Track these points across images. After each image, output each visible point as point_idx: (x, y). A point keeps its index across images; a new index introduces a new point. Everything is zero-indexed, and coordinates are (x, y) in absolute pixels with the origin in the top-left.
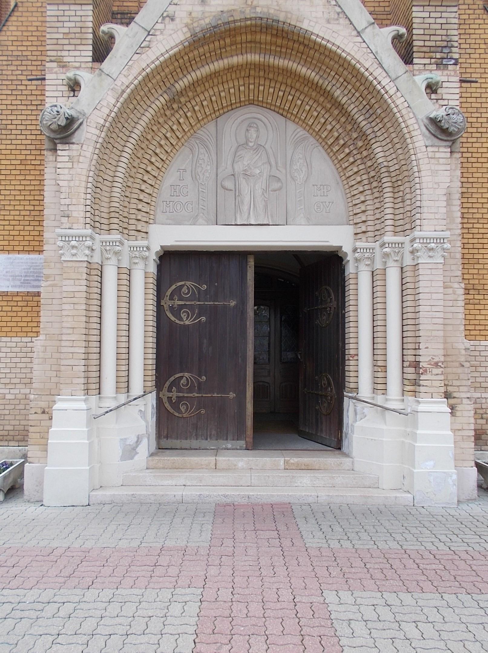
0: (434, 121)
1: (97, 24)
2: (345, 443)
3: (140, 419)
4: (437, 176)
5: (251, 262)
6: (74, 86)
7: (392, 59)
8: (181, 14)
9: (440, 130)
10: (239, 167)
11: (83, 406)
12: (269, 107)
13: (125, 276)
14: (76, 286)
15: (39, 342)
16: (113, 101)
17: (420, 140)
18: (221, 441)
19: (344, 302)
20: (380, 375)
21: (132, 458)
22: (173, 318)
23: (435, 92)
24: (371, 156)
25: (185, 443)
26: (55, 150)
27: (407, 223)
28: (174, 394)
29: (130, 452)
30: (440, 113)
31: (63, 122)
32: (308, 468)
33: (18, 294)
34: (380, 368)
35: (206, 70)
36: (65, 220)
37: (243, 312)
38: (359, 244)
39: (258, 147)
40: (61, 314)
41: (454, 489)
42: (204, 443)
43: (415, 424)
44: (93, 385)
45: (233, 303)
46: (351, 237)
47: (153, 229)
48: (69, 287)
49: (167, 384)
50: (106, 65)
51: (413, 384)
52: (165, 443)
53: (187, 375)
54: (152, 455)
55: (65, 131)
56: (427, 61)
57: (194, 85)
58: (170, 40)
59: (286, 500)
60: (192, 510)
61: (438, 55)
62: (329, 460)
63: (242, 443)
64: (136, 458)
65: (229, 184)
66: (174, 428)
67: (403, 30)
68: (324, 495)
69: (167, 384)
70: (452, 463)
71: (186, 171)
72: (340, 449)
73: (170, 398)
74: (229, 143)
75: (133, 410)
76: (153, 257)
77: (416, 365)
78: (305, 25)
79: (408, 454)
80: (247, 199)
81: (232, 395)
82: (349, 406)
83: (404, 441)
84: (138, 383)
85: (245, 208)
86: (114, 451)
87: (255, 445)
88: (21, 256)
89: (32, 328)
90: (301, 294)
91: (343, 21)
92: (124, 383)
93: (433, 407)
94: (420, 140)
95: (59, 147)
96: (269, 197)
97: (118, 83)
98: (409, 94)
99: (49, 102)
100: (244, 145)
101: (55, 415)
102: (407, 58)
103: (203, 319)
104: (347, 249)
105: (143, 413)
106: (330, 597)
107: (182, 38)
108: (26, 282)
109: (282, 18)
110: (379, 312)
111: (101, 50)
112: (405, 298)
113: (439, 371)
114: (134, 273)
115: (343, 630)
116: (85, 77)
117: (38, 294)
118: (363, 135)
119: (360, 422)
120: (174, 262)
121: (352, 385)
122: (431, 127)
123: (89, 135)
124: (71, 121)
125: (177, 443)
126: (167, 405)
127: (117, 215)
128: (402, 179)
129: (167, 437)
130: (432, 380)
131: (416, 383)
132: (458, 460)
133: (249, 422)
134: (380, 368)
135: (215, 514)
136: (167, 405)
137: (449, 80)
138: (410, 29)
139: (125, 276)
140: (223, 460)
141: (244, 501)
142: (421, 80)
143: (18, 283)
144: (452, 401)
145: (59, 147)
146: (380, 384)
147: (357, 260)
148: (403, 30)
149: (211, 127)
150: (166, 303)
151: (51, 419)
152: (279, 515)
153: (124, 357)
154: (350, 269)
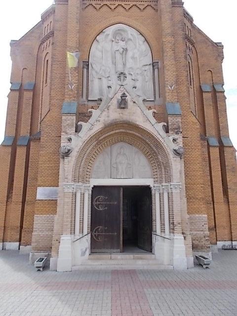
0: (175, 150)
1: (78, 121)
2: (153, 250)
3: (86, 242)
4: (177, 166)
5: (122, 190)
6: (70, 140)
7: (163, 133)
8: (102, 119)
9: (176, 152)
10: (118, 161)
11: (70, 238)
12: (125, 142)
13: (83, 195)
14: (68, 200)
15: (56, 217)
16: (81, 144)
17: (171, 155)
18: (112, 250)
19: (151, 202)
20: (163, 227)
21: (84, 255)
22: (96, 208)
23: (176, 141)
24: (158, 159)
25: (100, 251)
26: (64, 158)
27: (169, 179)
28: (97, 234)
29: (83, 254)
30: (176, 148)
31: (67, 151)
32: (141, 259)
33: (46, 200)
34: (163, 224)
35: (108, 134)
36: (66, 180)
37: (119, 206)
38: (155, 185)
39: (124, 154)
40: (63, 207)
41: (186, 264)
42: (107, 251)
43: (173, 243)
44: (73, 232)
45: (116, 203)
46: (153, 182)
47: (91, 180)
48: (66, 200)
49: (94, 230)
50: (80, 134)
51: (172, 230)
52: (94, 251)
53: (101, 227)
54: (90, 255)
55: (67, 153)
56: (173, 132)
57: (104, 138)
58: (98, 127)
59: (134, 269)
60: (105, 272)
61: (176, 131)
62: (148, 256)
63: (119, 250)
64: (86, 255)
65: (115, 166)
66: (96, 246)
67: (166, 124)
68: (146, 267)
69: (94, 230)
70: (185, 256)
71: (101, 162)
72: (151, 252)
73: (95, 235)
74: (114, 154)
75: (84, 239)
76: (91, 189)
77: (173, 223)
78: (137, 123)
79: (171, 253)
80: (120, 171)
81: (116, 234)
82: (154, 236)
83: (171, 249)
84: (86, 230)
85: (120, 173)
86: (79, 253)
87: (123, 251)
88: (47, 188)
89: (54, 212)
90: (138, 202)
91: (148, 122)
92: (82, 231)
93: (179, 237)
94: (171, 155)
95: (65, 158)
96: (128, 171)
97: (83, 139)
98: (169, 143)
99: (62, 145)
100: (119, 154)
101: (61, 241)
102: (167, 132)
103: (106, 208)
104: (152, 186)
105: (87, 240)
106: (145, 290)
107: (102, 126)
108: (49, 196)
109: (130, 121)
110: (171, 199)
111: (78, 129)
112: (170, 201)
113: (180, 225)
114: (85, 195)
115: (148, 296)
116: (73, 137)
117: (56, 200)
118: (155, 152)
119: (158, 243)
120: (97, 190)
121: (154, 230)
122: (174, 152)
123: (74, 154)
124: (69, 150)
125: (97, 251)
126: (94, 238)
127: (80, 177)
128: (167, 167)
129: (94, 249)
130: (178, 228)
131: (173, 229)
132: (187, 255)
133: (121, 243)
134: (163, 224)
135: (112, 273)
136: (94, 238)
137: (179, 138)
138: (167, 123)
139: (83, 195)
140: (113, 256)
141: (121, 269)
142: (171, 138)
143: (46, 197)
144: (184, 235)
145: (65, 158)
146: (163, 230)
147: (155, 190)
148: (166, 124)
149: (109, 148)
150: (94, 203)
151: (60, 242)
152: (132, 273)
153: (82, 222)
154: (153, 192)
